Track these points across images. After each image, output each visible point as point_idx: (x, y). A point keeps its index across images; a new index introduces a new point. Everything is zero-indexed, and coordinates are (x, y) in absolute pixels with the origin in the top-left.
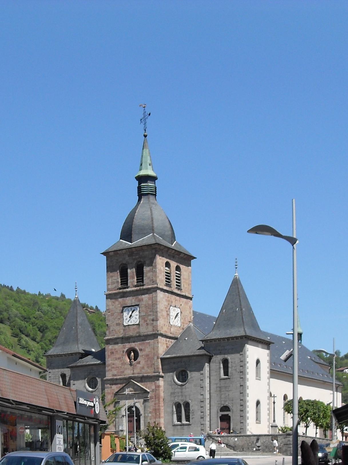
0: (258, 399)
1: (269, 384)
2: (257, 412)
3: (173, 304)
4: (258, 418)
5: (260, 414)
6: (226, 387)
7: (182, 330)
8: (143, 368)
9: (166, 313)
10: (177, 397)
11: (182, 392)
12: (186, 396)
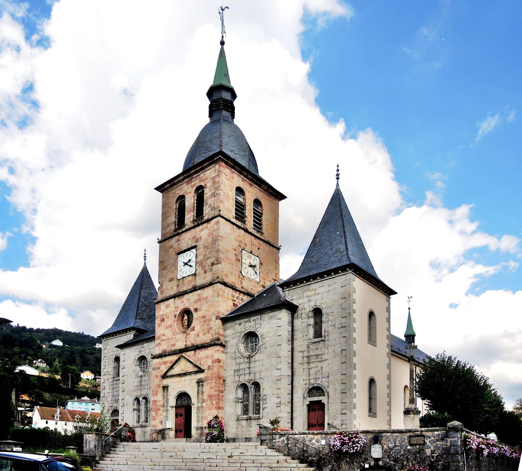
0: (371, 376)
1: (389, 366)
2: (370, 399)
3: (248, 248)
4: (372, 407)
5: (376, 402)
6: (317, 356)
7: (262, 288)
8: (198, 335)
10: (242, 377)
11: (249, 368)
12: (255, 373)
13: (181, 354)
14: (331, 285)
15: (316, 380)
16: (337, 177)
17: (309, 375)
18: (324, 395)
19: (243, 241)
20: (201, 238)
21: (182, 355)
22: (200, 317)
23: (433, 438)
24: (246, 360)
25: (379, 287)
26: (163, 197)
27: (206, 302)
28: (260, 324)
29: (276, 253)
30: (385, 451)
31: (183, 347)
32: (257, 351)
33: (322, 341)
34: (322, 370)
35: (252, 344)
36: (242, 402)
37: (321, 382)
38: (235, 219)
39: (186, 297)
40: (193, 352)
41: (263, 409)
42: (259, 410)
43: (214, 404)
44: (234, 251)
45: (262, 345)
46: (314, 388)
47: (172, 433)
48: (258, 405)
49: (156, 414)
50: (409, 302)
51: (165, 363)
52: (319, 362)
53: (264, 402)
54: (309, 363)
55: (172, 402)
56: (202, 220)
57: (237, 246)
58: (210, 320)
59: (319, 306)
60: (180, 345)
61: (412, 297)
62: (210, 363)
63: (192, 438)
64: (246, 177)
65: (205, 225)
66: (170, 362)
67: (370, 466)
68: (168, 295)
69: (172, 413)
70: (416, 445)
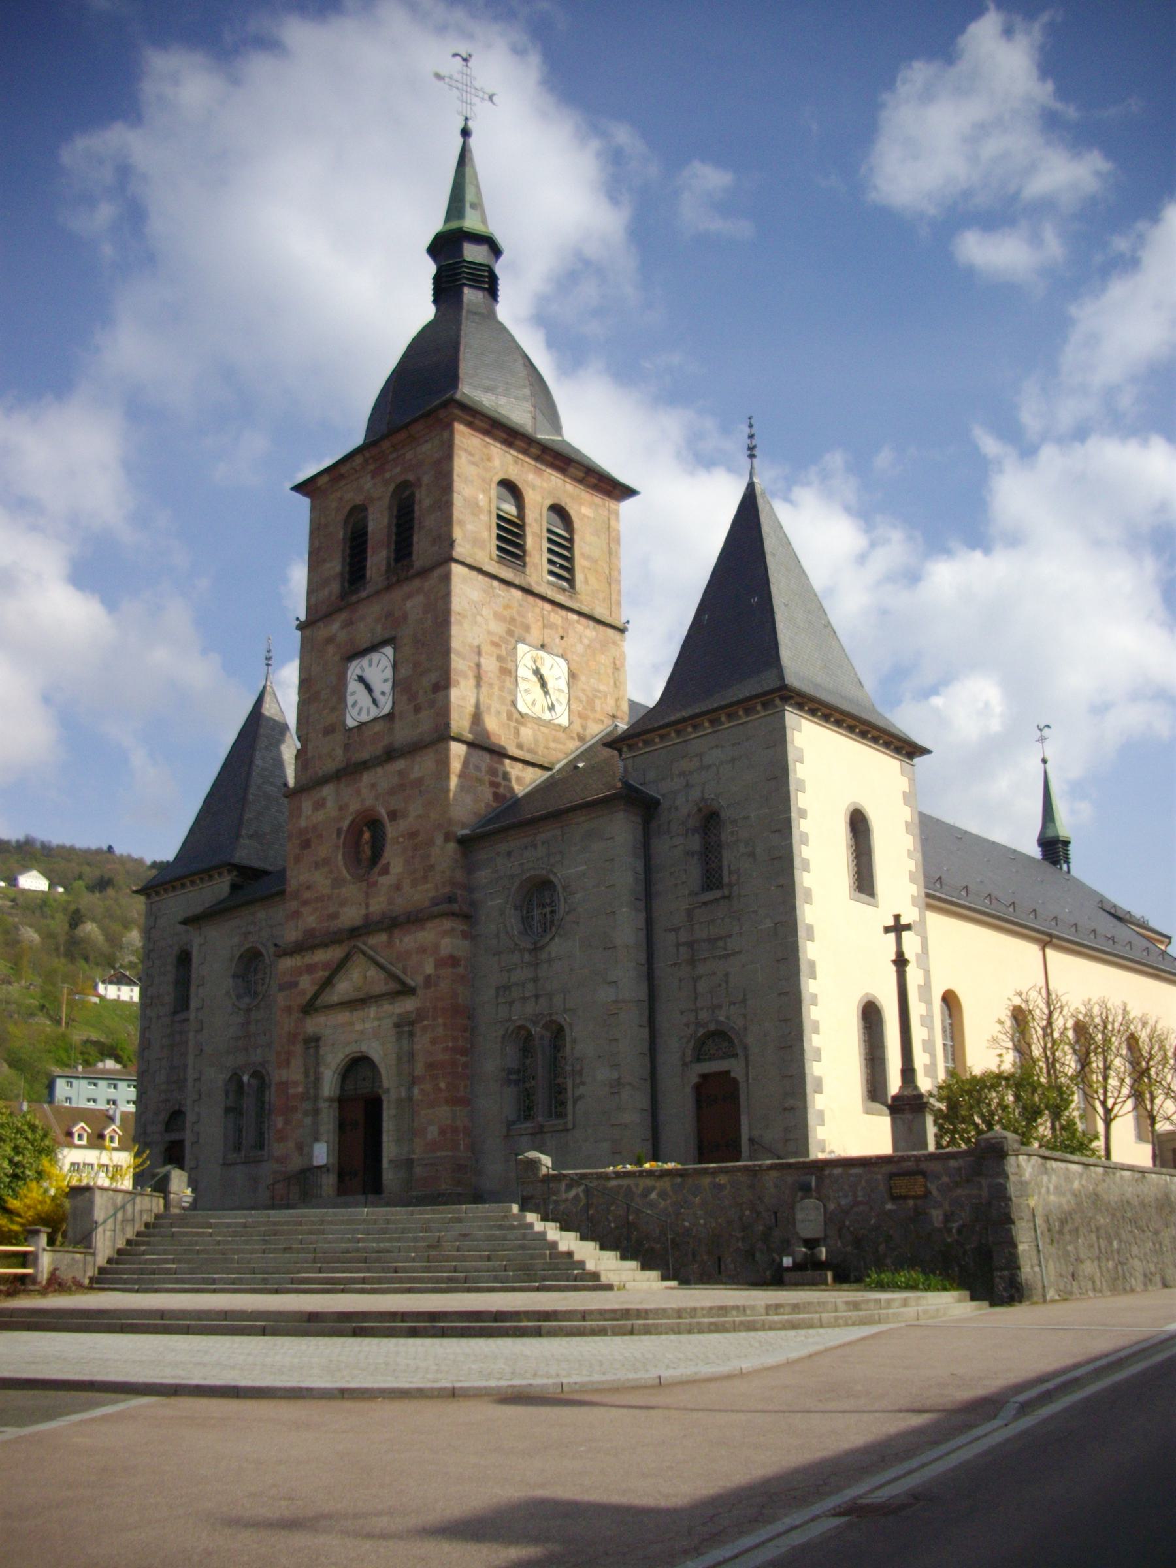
6: (712, 941)
7: (577, 743)
8: (398, 887)
9: (498, 664)
11: (535, 980)
13: (353, 943)
14: (739, 744)
15: (713, 1012)
16: (749, 452)
17: (696, 998)
18: (735, 1055)
19: (519, 619)
20: (405, 617)
21: (355, 946)
22: (403, 836)
23: (945, 1179)
24: (527, 957)
25: (875, 740)
26: (313, 509)
27: (420, 791)
28: (561, 852)
29: (614, 643)
30: (829, 1219)
31: (358, 922)
32: (554, 929)
33: (724, 897)
34: (727, 982)
35: (544, 911)
36: (517, 1082)
37: (727, 1018)
38: (498, 562)
39: (367, 778)
40: (383, 937)
41: (575, 1103)
42: (563, 1104)
43: (440, 1090)
44: (493, 649)
45: (568, 913)
46: (711, 1035)
47: (329, 1182)
48: (560, 1090)
49: (287, 1122)
50: (1042, 740)
51: (311, 969)
52: (720, 957)
53: (578, 1081)
54: (692, 962)
55: (329, 1085)
56: (408, 571)
57: (504, 634)
58: (430, 843)
59: (713, 799)
60: (351, 915)
61: (1048, 726)
62: (429, 969)
63: (383, 1195)
64: (525, 452)
65: (417, 583)
66: (326, 965)
67: (794, 1262)
68: (320, 773)
69: (328, 1119)
70: (905, 1198)
